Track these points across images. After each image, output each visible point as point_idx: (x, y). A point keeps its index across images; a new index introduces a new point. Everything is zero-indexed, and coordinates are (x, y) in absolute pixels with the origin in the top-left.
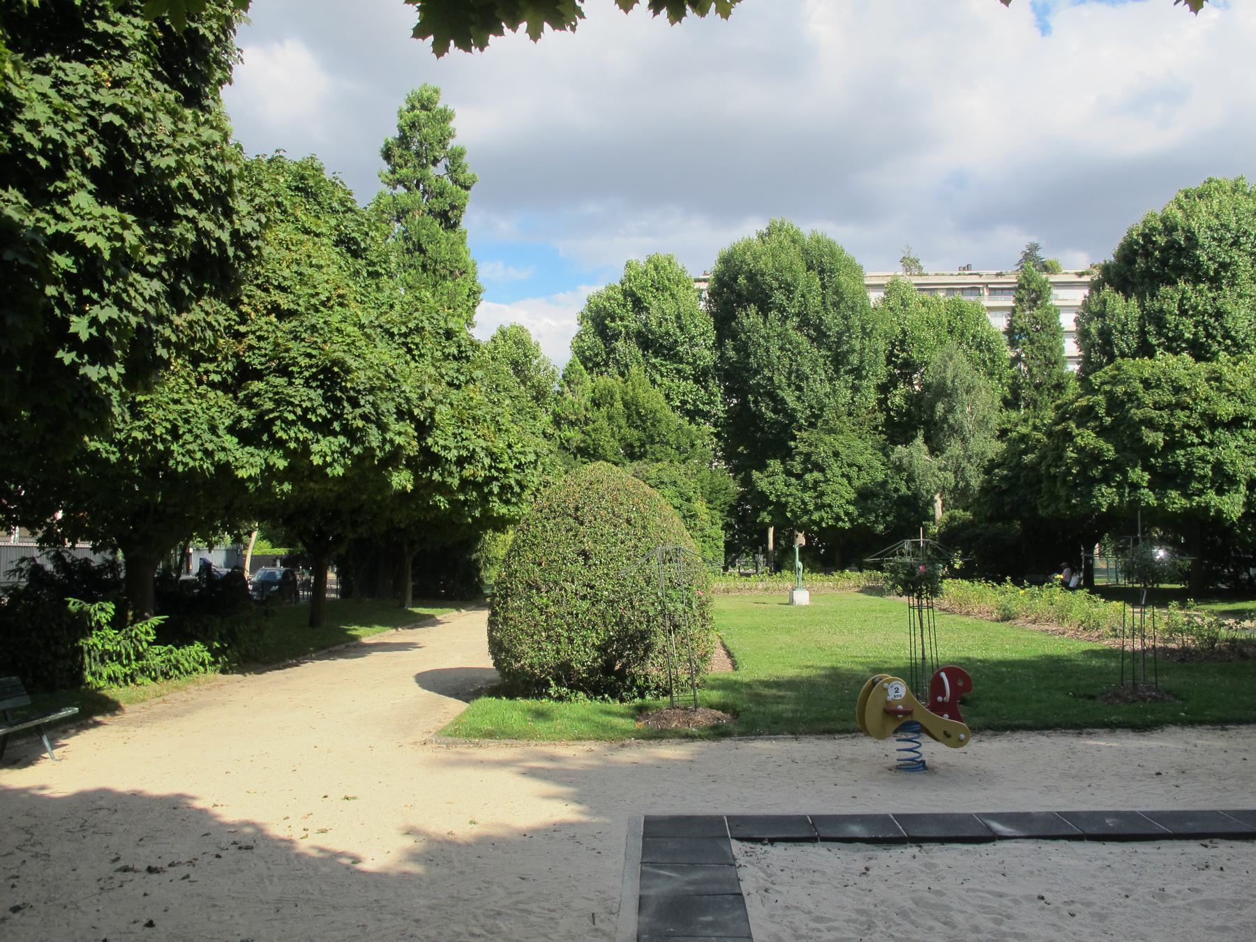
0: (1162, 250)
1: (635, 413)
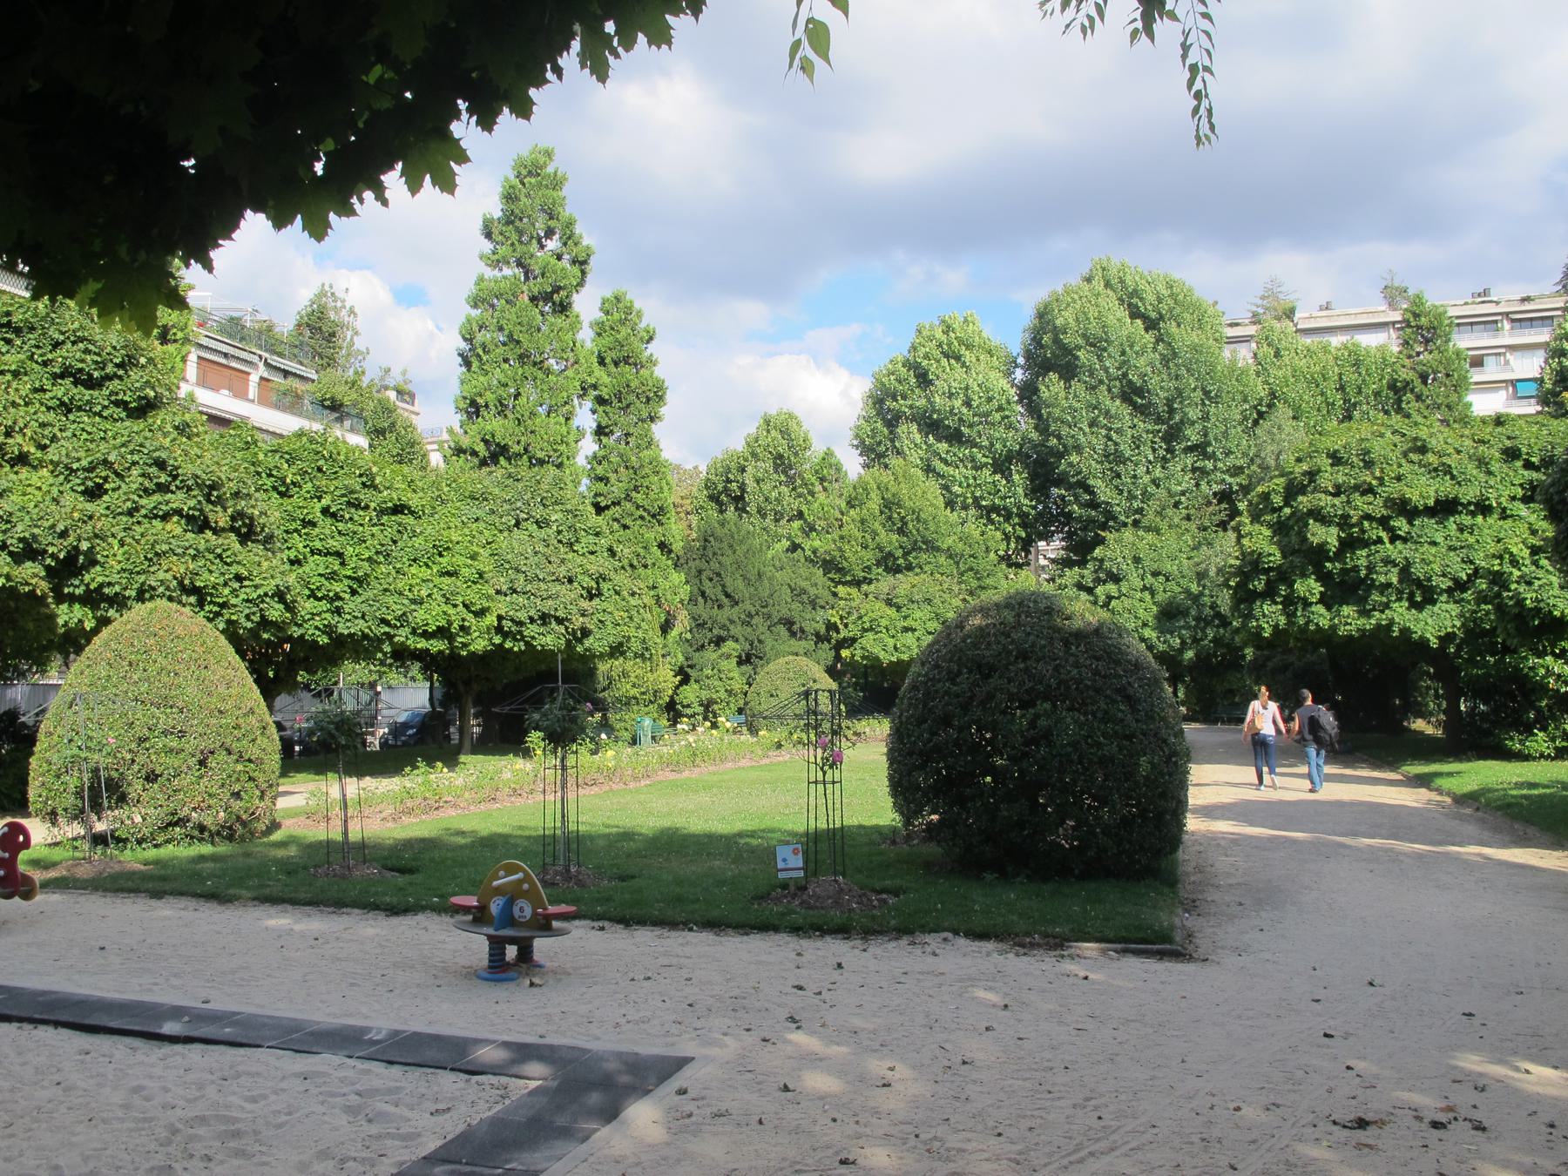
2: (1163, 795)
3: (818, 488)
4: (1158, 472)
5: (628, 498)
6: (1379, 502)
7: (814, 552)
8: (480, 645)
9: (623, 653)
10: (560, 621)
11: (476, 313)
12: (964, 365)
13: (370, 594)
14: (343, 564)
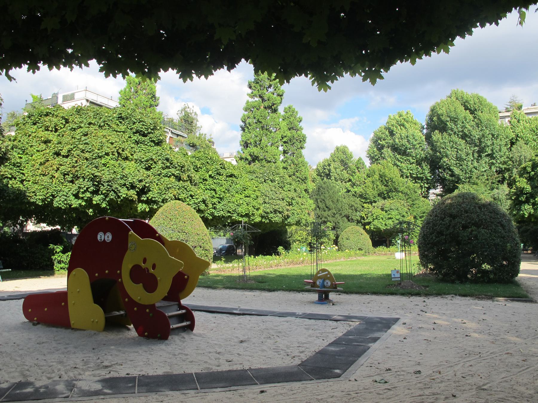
2: (515, 256)
3: (356, 171)
4: (476, 164)
5: (294, 175)
8: (258, 219)
9: (300, 224)
10: (280, 213)
11: (246, 113)
12: (405, 128)
14: (216, 193)
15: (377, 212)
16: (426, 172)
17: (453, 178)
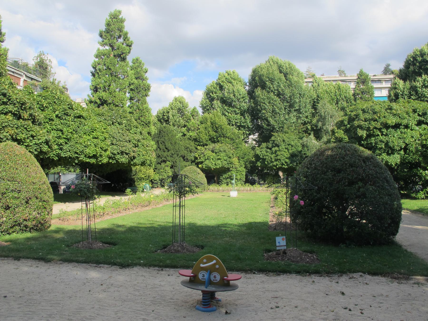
0: (420, 63)
1: (215, 127)
3: (192, 118)
4: (287, 117)
6: (379, 124)
7: (190, 136)
9: (145, 164)
10: (127, 154)
11: (97, 60)
13: (72, 143)
14: (63, 134)
15: (208, 153)
16: (248, 121)
17: (269, 128)
